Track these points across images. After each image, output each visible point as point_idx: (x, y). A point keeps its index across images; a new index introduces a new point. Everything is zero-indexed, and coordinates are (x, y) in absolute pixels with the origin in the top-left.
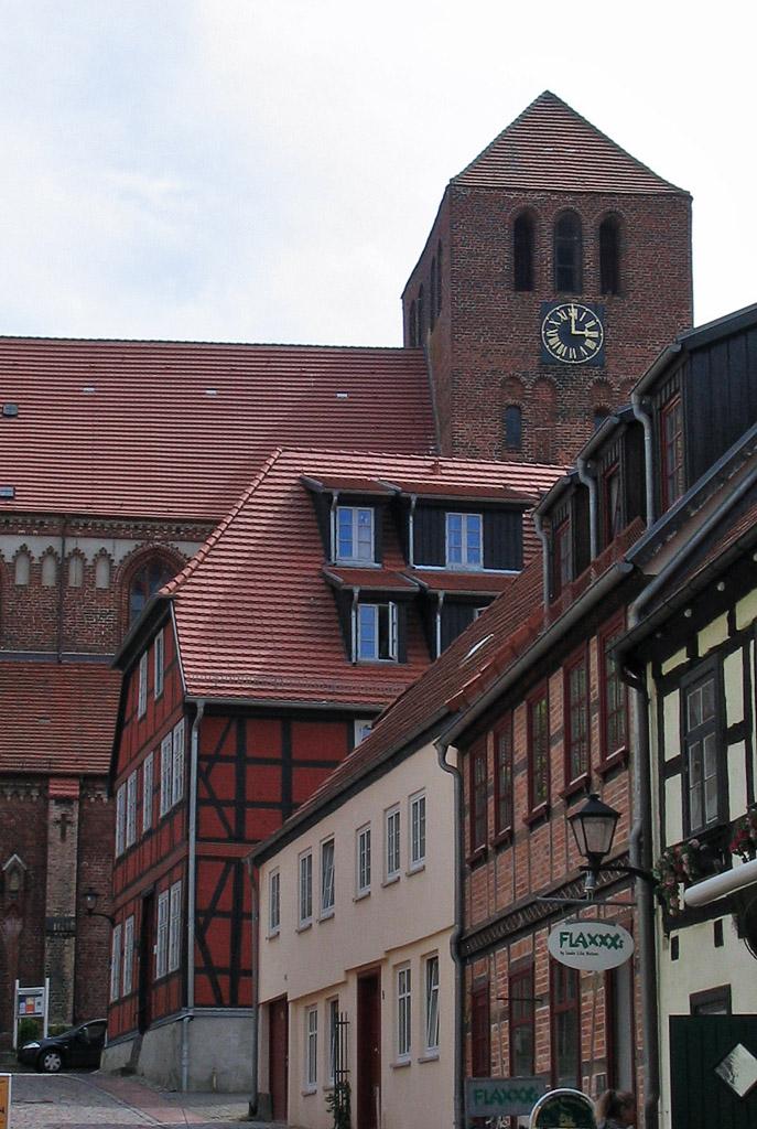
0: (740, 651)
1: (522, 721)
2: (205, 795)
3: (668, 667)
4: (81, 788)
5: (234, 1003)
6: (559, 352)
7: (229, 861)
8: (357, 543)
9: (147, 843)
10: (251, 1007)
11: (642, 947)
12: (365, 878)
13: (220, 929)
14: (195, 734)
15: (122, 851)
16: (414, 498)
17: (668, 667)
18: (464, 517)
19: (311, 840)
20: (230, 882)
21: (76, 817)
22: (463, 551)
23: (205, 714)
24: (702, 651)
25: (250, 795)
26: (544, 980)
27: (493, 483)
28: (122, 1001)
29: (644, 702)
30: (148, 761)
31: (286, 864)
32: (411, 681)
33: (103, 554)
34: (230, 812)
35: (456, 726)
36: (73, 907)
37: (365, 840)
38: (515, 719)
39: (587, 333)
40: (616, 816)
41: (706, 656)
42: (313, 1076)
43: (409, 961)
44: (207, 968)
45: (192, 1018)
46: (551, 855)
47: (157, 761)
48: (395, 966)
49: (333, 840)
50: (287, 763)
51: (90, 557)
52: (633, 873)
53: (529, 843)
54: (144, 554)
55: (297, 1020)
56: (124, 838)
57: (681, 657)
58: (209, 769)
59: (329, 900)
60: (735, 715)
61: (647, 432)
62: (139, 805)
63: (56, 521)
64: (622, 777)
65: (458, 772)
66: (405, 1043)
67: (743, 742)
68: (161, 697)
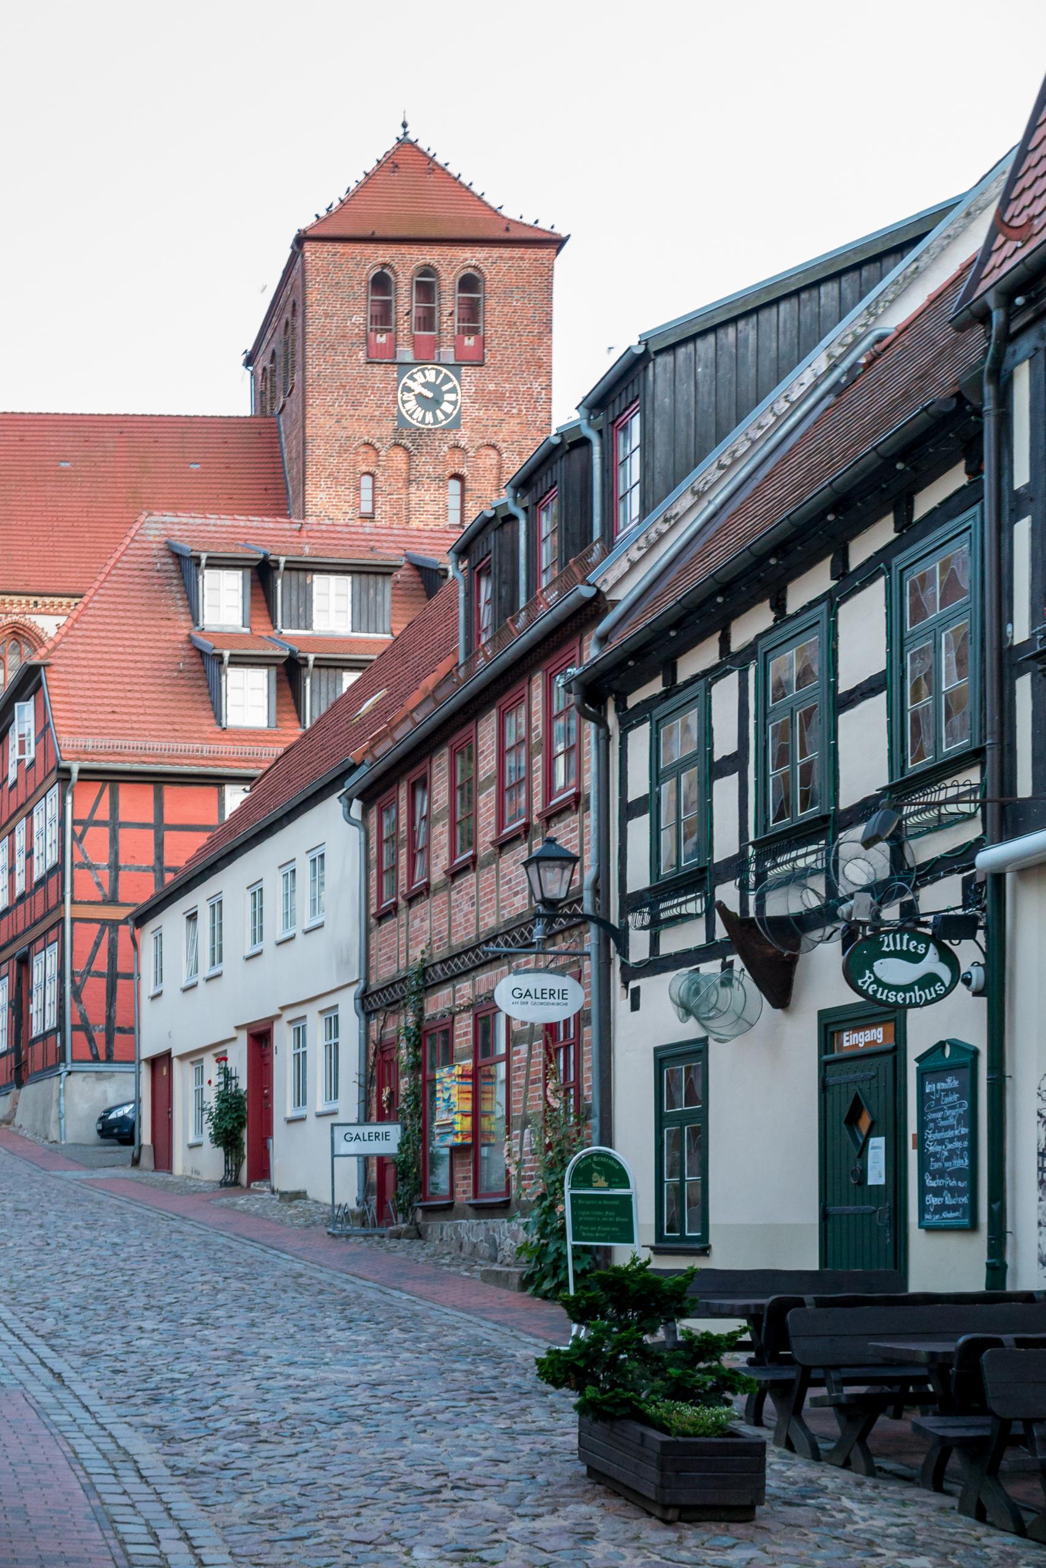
0: (734, 677)
1: (443, 769)
3: (633, 700)
5: (109, 1059)
6: (415, 416)
7: (104, 922)
8: (224, 600)
9: (21, 907)
10: (133, 1062)
11: (594, 999)
12: (258, 934)
13: (96, 988)
17: (633, 700)
22: (331, 609)
23: (79, 780)
24: (682, 676)
26: (465, 1034)
29: (604, 739)
34: (105, 876)
38: (434, 766)
40: (574, 859)
41: (688, 683)
42: (333, 1092)
43: (336, 1006)
45: (70, 1073)
46: (506, 891)
48: (290, 1022)
49: (196, 913)
50: (159, 827)
52: (586, 919)
53: (449, 896)
55: (182, 1077)
58: (84, 832)
60: (725, 744)
61: (596, 449)
64: (572, 820)
65: (364, 823)
66: (301, 1098)
67: (736, 775)
68: (15, 783)
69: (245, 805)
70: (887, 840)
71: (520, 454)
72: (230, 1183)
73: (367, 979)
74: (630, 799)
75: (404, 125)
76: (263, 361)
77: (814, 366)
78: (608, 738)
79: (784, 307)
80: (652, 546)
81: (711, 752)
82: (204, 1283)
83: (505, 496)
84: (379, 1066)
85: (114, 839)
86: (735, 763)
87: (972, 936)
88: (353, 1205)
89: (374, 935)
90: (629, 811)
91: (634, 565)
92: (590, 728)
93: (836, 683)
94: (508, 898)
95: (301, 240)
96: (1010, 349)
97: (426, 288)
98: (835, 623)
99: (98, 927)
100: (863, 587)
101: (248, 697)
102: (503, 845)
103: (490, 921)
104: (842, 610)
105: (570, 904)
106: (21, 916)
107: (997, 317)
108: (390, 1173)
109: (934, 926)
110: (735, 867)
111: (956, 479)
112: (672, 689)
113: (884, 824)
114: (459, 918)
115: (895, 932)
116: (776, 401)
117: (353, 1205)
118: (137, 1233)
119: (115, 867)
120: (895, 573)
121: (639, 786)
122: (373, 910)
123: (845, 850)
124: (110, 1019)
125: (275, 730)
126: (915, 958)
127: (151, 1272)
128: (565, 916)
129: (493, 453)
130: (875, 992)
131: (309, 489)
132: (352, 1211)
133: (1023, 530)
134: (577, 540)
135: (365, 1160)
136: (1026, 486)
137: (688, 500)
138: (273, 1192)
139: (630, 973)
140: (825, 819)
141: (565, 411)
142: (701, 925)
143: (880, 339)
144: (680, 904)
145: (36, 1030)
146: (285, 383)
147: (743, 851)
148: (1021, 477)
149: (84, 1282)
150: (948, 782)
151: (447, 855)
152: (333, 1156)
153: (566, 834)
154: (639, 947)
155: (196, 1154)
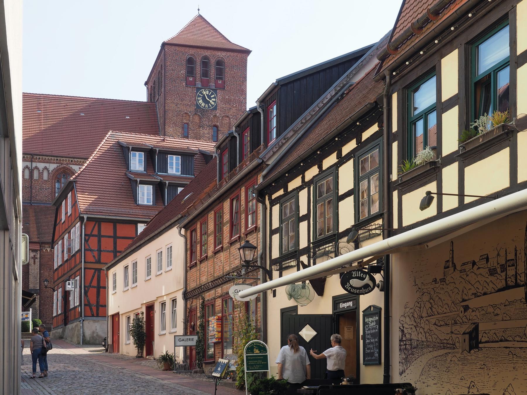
0: (306, 189)
2: (87, 247)
3: (274, 196)
4: (40, 247)
5: (98, 316)
7: (96, 269)
8: (137, 163)
9: (66, 264)
12: (149, 273)
13: (93, 292)
14: (83, 227)
16: (157, 149)
17: (274, 196)
18: (174, 157)
19: (129, 261)
21: (38, 256)
22: (174, 167)
26: (219, 305)
27: (185, 146)
28: (58, 315)
29: (265, 209)
30: (66, 236)
31: (118, 270)
32: (161, 209)
33: (45, 168)
34: (96, 254)
35: (186, 221)
36: (38, 286)
37: (149, 261)
39: (211, 101)
40: (255, 248)
41: (291, 191)
44: (88, 304)
46: (232, 258)
47: (69, 237)
50: (115, 237)
51: (41, 169)
54: (60, 169)
56: (57, 262)
57: (281, 192)
59: (135, 281)
60: (303, 211)
61: (262, 115)
62: (63, 251)
63: (29, 156)
64: (254, 235)
65: (185, 237)
68: (64, 221)
69: (145, 230)
70: (353, 242)
71: (236, 119)
72: (140, 357)
73: (186, 288)
74: (273, 228)
75: (199, 10)
76: (151, 84)
77: (331, 93)
78: (266, 208)
79: (321, 74)
80: (280, 147)
81: (299, 213)
82: (131, 389)
85: (99, 241)
86: (306, 217)
87: (380, 273)
88: (181, 363)
89: (189, 273)
90: (273, 232)
92: (260, 205)
93: (338, 192)
94: (233, 261)
95: (164, 45)
96: (391, 88)
98: (338, 173)
99: (93, 271)
100: (346, 162)
101: (145, 194)
102: (232, 244)
104: (340, 169)
105: (254, 263)
106: (66, 267)
107: (388, 78)
108: (194, 352)
109: (368, 269)
110: (306, 251)
111: (375, 128)
112: (286, 193)
113: (353, 237)
114: (217, 267)
115: (356, 271)
116: (319, 103)
117: (181, 363)
118: (108, 373)
119: (100, 250)
120: (356, 157)
122: (188, 265)
123: (340, 245)
124: (98, 302)
125: (155, 206)
126: (363, 279)
127: (112, 385)
128: (252, 266)
129: (227, 119)
130: (350, 289)
131: (167, 127)
132: (181, 365)
133: (395, 145)
134: (255, 144)
135: (185, 348)
136: (396, 132)
137: (291, 133)
138: (154, 359)
140: (334, 235)
141: (251, 102)
143: (351, 86)
144: (289, 263)
145: (72, 307)
146: (158, 92)
147: (309, 245)
149: (89, 389)
150: (373, 224)
151: (213, 246)
152: (175, 346)
155: (128, 346)
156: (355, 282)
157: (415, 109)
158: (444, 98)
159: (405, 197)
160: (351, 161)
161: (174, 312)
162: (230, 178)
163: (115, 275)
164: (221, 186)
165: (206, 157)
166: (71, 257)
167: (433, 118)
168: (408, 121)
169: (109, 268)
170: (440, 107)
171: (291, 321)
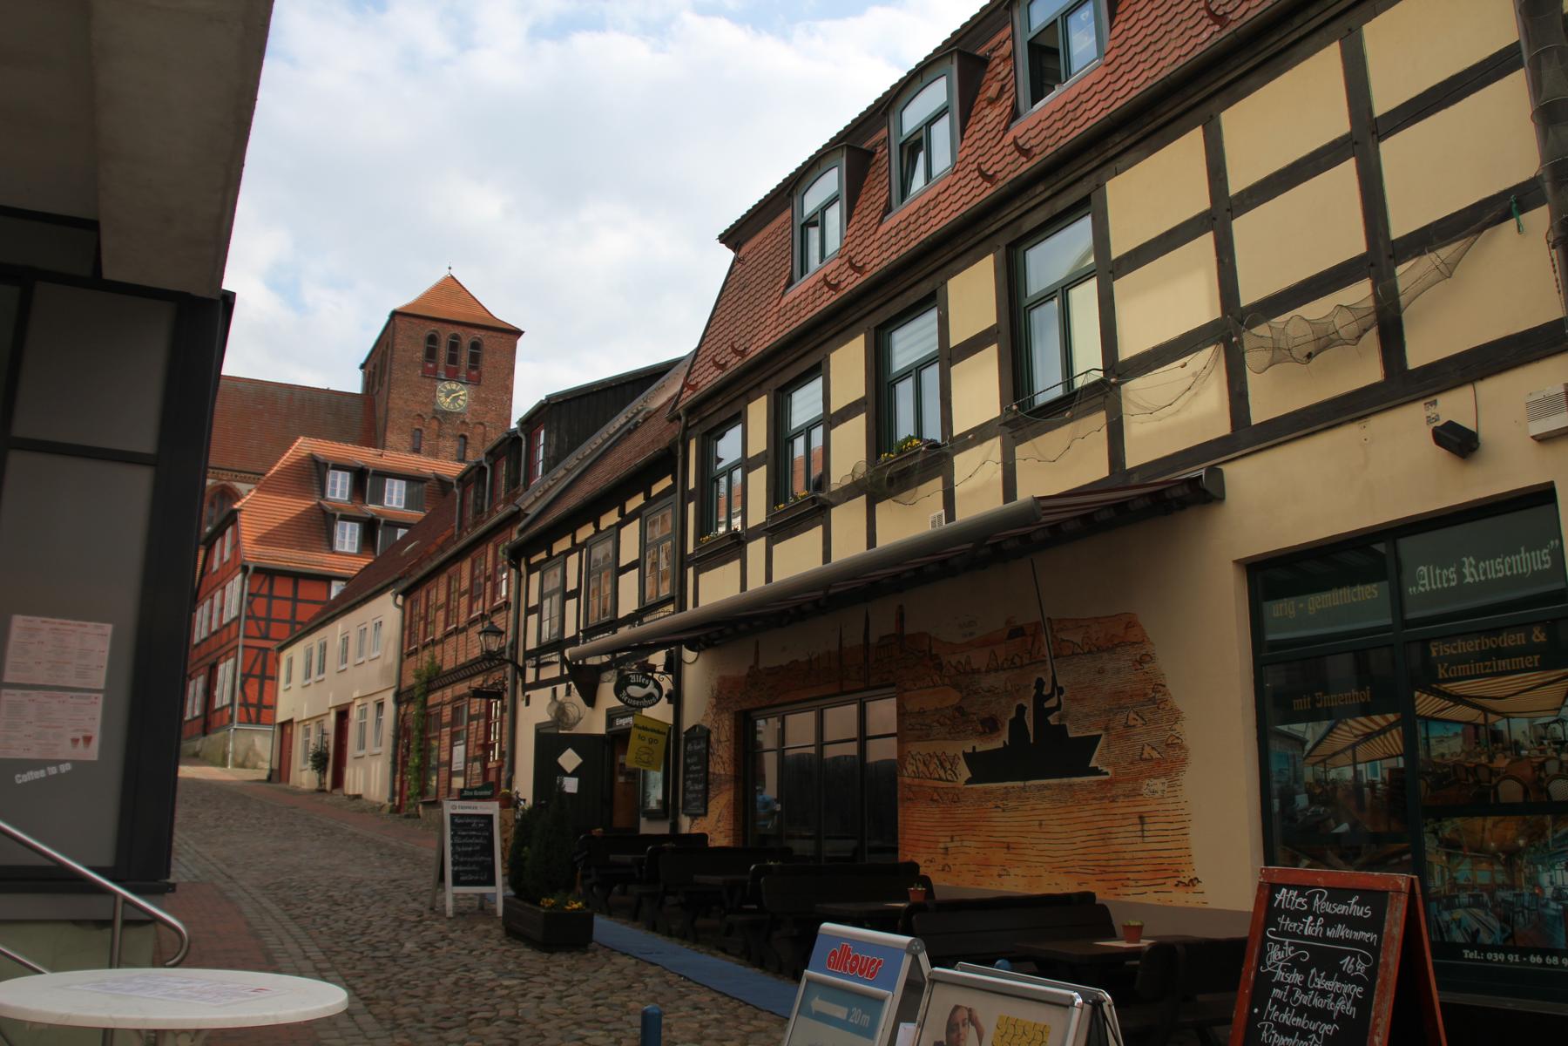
3: (534, 560)
5: (258, 722)
7: (260, 649)
8: (339, 487)
15: (204, 634)
17: (534, 560)
19: (314, 640)
20: (260, 661)
22: (395, 496)
24: (555, 553)
25: (273, 615)
28: (195, 718)
30: (218, 595)
31: (297, 652)
35: (404, 585)
44: (245, 704)
50: (295, 600)
52: (507, 661)
55: (298, 735)
57: (543, 555)
59: (322, 670)
60: (572, 585)
64: (504, 613)
65: (403, 608)
66: (362, 746)
73: (400, 685)
78: (521, 577)
80: (546, 491)
83: (483, 457)
84: (401, 731)
90: (530, 611)
91: (537, 499)
97: (454, 346)
101: (347, 537)
103: (462, 660)
111: (667, 482)
112: (550, 557)
114: (447, 657)
121: (533, 601)
126: (644, 686)
133: (691, 507)
137: (562, 472)
139: (527, 687)
142: (558, 667)
145: (217, 706)
148: (692, 485)
153: (499, 621)
154: (530, 676)
156: (635, 691)
157: (719, 460)
158: (835, 406)
159: (702, 577)
160: (637, 522)
161: (379, 722)
162: (475, 525)
163: (290, 661)
164: (460, 537)
165: (443, 484)
166: (223, 627)
167: (817, 435)
168: (708, 478)
169: (282, 649)
170: (747, 464)
171: (549, 743)
